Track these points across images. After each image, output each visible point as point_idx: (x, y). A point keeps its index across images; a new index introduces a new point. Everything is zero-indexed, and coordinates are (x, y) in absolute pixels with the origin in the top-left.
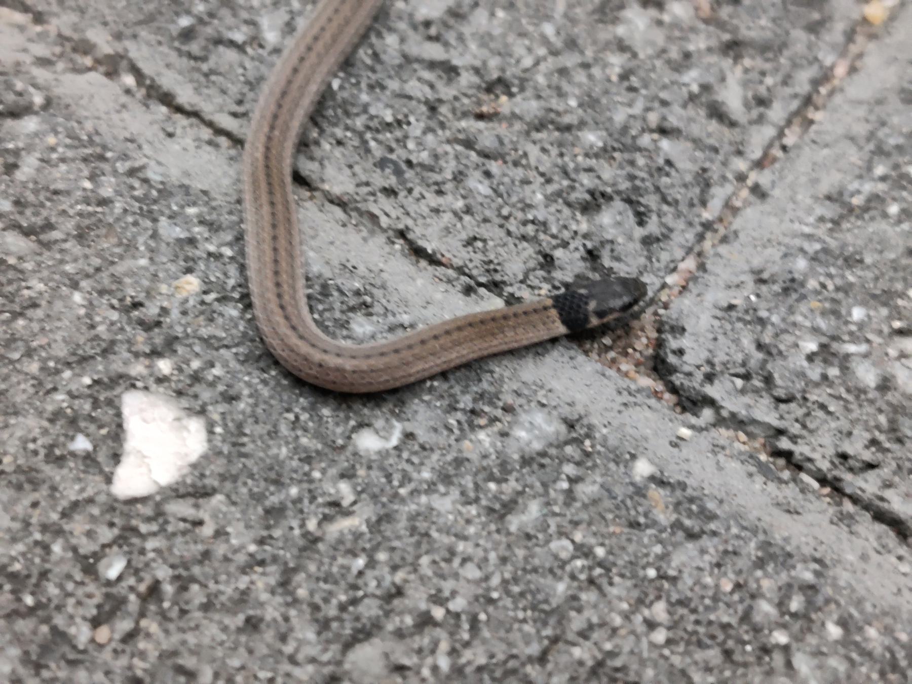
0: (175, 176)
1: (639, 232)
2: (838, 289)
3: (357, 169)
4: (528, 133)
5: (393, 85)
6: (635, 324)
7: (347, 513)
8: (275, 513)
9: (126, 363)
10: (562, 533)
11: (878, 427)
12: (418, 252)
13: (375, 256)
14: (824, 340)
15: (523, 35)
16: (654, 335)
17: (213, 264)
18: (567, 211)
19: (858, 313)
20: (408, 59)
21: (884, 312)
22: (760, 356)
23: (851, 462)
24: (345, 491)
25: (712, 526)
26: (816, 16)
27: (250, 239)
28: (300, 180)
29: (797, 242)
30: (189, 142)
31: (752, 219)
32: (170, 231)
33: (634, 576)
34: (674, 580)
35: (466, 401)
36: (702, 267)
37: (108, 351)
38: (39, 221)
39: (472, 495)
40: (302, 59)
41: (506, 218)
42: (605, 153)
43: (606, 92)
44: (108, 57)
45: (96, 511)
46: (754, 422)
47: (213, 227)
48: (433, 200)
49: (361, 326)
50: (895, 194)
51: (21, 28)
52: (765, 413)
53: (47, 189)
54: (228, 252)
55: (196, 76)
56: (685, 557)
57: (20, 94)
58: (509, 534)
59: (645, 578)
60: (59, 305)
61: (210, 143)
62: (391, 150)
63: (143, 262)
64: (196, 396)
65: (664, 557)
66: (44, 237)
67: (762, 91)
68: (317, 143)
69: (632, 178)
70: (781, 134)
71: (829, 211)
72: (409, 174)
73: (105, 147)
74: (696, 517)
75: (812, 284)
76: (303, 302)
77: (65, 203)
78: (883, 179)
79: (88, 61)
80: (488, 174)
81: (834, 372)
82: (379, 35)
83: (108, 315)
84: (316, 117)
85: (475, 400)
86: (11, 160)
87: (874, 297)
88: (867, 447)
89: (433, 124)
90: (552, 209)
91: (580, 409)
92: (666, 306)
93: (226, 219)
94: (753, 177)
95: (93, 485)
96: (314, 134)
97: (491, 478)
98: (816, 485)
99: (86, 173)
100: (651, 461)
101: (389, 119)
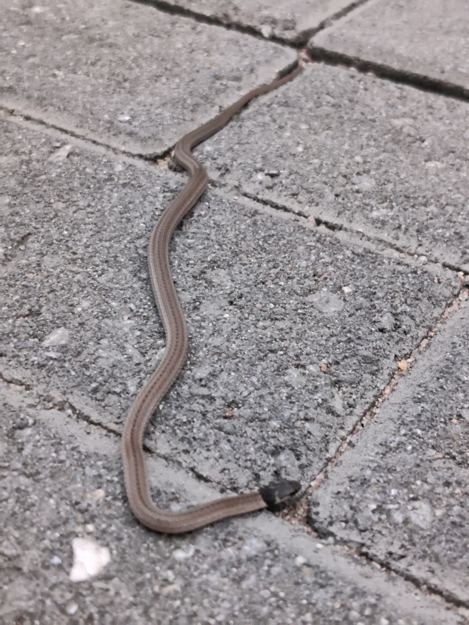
0: (92, 449)
1: (297, 463)
2: (385, 482)
3: (171, 442)
4: (247, 423)
5: (187, 406)
6: (298, 504)
7: (171, 583)
8: (140, 585)
9: (74, 527)
10: (266, 588)
11: (404, 539)
12: (200, 477)
13: (180, 479)
14: (379, 504)
15: (243, 382)
16: (306, 507)
17: (110, 485)
18: (265, 455)
19: (394, 492)
20: (192, 395)
21: (406, 491)
22: (352, 512)
23: (394, 556)
24: (170, 575)
25: (331, 582)
26: (375, 368)
27: (126, 475)
28: (147, 449)
29: (367, 464)
30: (97, 436)
31: (348, 455)
32: (91, 472)
33: (297, 603)
34: (314, 605)
35: (222, 536)
36: (326, 477)
37: (66, 522)
38: (33, 471)
39: (226, 573)
40: (146, 396)
41: (238, 459)
42: (281, 430)
43: (281, 404)
44: (59, 402)
45: (64, 587)
46: (351, 541)
47: (109, 469)
48: (205, 454)
49: (175, 507)
50: (410, 441)
51: (21, 392)
52: (355, 536)
53: (36, 457)
54: (116, 479)
55: (99, 408)
56: (320, 595)
57: (22, 419)
58: (242, 589)
59: (301, 604)
60: (44, 505)
61: (106, 435)
62: (186, 434)
63: (79, 485)
64: (104, 539)
65: (310, 595)
66: (36, 478)
67: (351, 401)
68: (153, 433)
69: (293, 439)
70: (361, 420)
71: (381, 450)
72: (194, 443)
73: (61, 439)
74: (323, 579)
75: (373, 480)
76: (150, 499)
77: (44, 463)
78: (405, 435)
79: (51, 405)
80: (229, 441)
81: (384, 517)
82: (180, 386)
83: (65, 508)
84: (153, 421)
85: (226, 535)
86: (20, 446)
87: (401, 484)
88: (400, 548)
89: (204, 421)
90: (258, 454)
91: (273, 537)
92: (311, 495)
93: (114, 466)
94: (349, 438)
95: (62, 576)
96: (152, 429)
97: (234, 566)
98: (379, 566)
99: (53, 450)
100: (304, 557)
101: (185, 420)
